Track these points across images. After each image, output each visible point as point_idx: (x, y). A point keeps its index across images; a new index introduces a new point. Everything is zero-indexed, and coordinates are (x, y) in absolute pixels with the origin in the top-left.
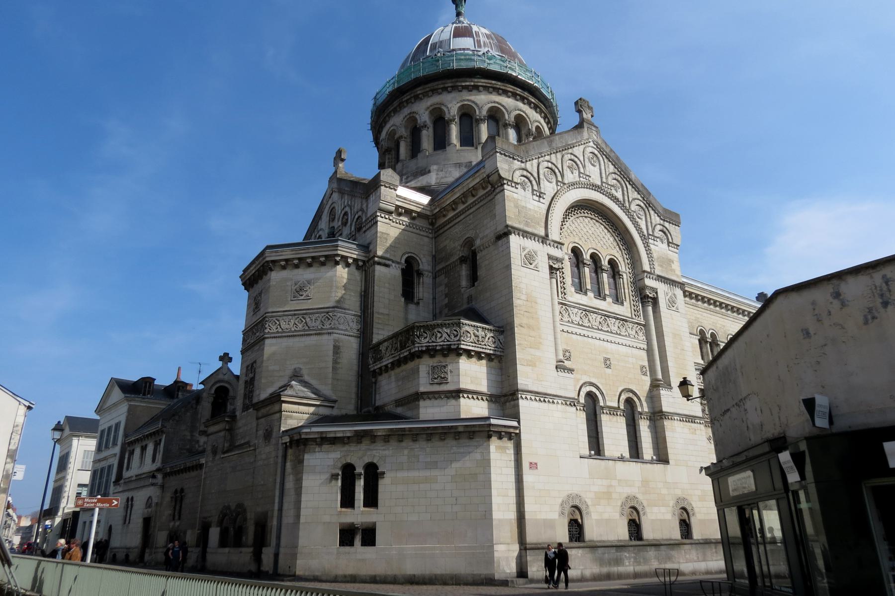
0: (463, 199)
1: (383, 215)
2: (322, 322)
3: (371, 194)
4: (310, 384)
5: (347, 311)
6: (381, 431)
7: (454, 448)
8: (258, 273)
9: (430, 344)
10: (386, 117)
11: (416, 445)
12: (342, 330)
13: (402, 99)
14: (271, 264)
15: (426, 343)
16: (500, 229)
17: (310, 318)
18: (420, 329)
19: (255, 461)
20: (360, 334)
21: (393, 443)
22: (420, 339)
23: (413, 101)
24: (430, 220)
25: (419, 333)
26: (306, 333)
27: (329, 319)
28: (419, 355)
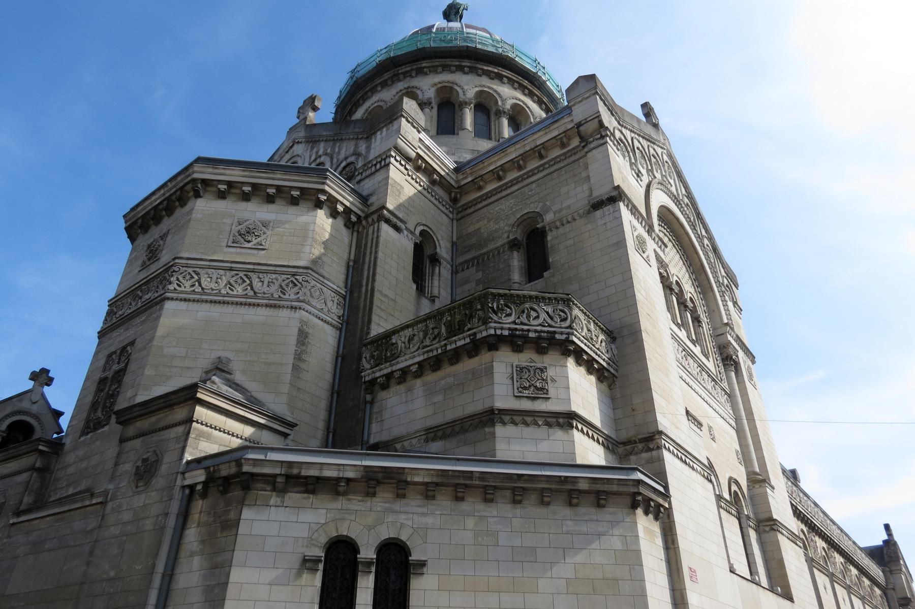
0: (521, 162)
1: (398, 158)
2: (281, 286)
3: (379, 130)
4: (243, 388)
5: (325, 281)
6: (422, 472)
7: (569, 523)
8: (168, 203)
9: (517, 327)
10: (367, 91)
11: (491, 511)
12: (315, 308)
13: (399, 70)
14: (199, 186)
15: (509, 323)
16: (601, 192)
17: (259, 277)
18: (498, 299)
19: (99, 527)
20: (342, 324)
21: (444, 503)
22: (500, 315)
23: (414, 74)
24: (453, 194)
25: (498, 307)
26: (249, 300)
27: (296, 285)
28: (494, 343)
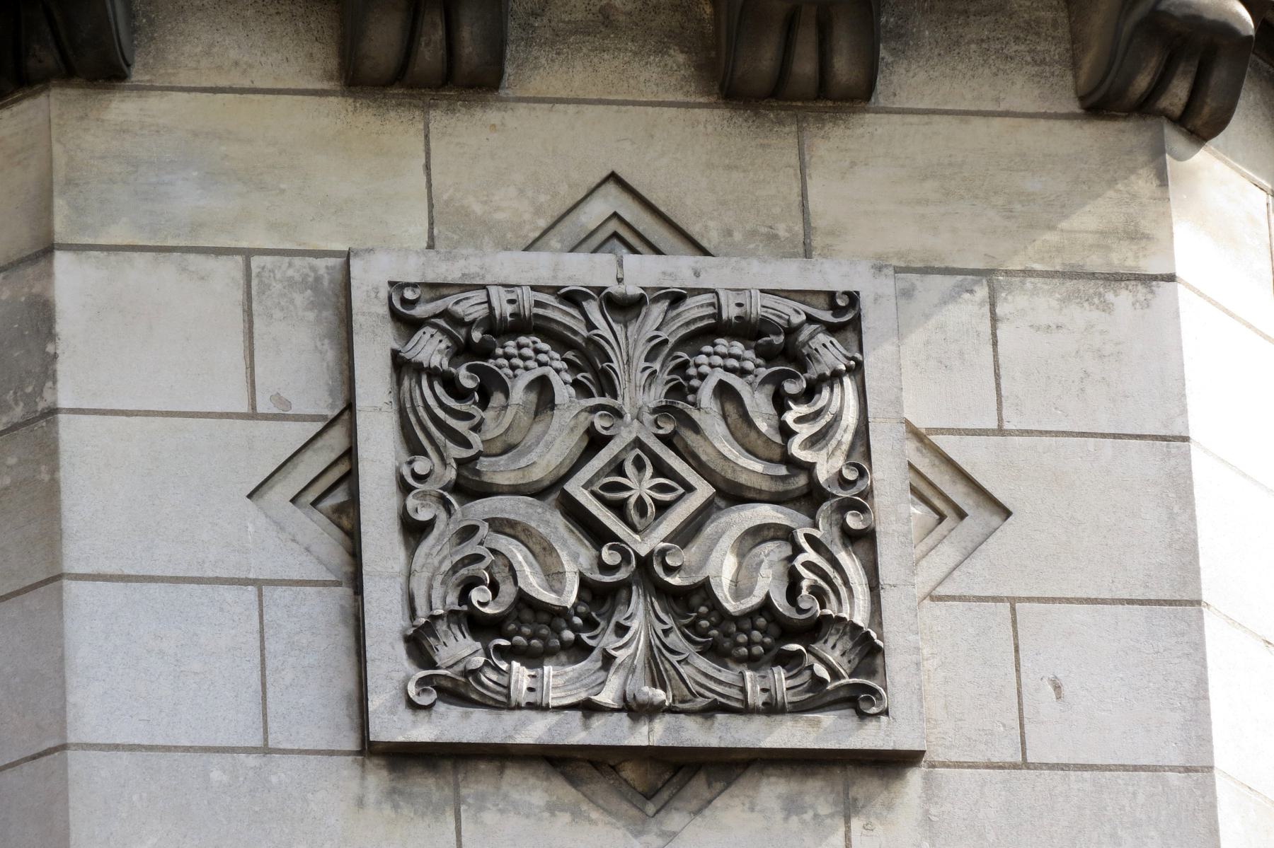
23: (1034, 275)
